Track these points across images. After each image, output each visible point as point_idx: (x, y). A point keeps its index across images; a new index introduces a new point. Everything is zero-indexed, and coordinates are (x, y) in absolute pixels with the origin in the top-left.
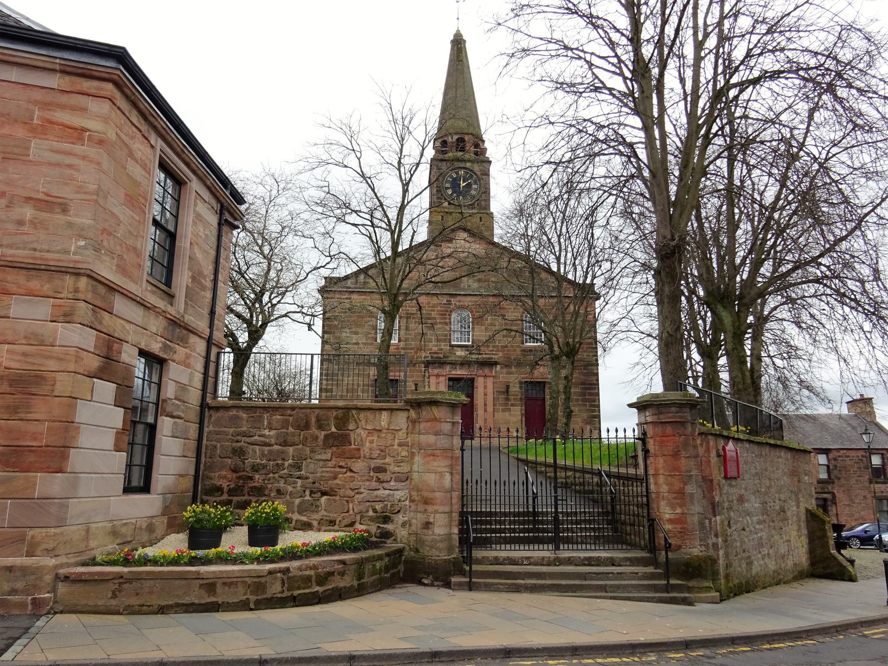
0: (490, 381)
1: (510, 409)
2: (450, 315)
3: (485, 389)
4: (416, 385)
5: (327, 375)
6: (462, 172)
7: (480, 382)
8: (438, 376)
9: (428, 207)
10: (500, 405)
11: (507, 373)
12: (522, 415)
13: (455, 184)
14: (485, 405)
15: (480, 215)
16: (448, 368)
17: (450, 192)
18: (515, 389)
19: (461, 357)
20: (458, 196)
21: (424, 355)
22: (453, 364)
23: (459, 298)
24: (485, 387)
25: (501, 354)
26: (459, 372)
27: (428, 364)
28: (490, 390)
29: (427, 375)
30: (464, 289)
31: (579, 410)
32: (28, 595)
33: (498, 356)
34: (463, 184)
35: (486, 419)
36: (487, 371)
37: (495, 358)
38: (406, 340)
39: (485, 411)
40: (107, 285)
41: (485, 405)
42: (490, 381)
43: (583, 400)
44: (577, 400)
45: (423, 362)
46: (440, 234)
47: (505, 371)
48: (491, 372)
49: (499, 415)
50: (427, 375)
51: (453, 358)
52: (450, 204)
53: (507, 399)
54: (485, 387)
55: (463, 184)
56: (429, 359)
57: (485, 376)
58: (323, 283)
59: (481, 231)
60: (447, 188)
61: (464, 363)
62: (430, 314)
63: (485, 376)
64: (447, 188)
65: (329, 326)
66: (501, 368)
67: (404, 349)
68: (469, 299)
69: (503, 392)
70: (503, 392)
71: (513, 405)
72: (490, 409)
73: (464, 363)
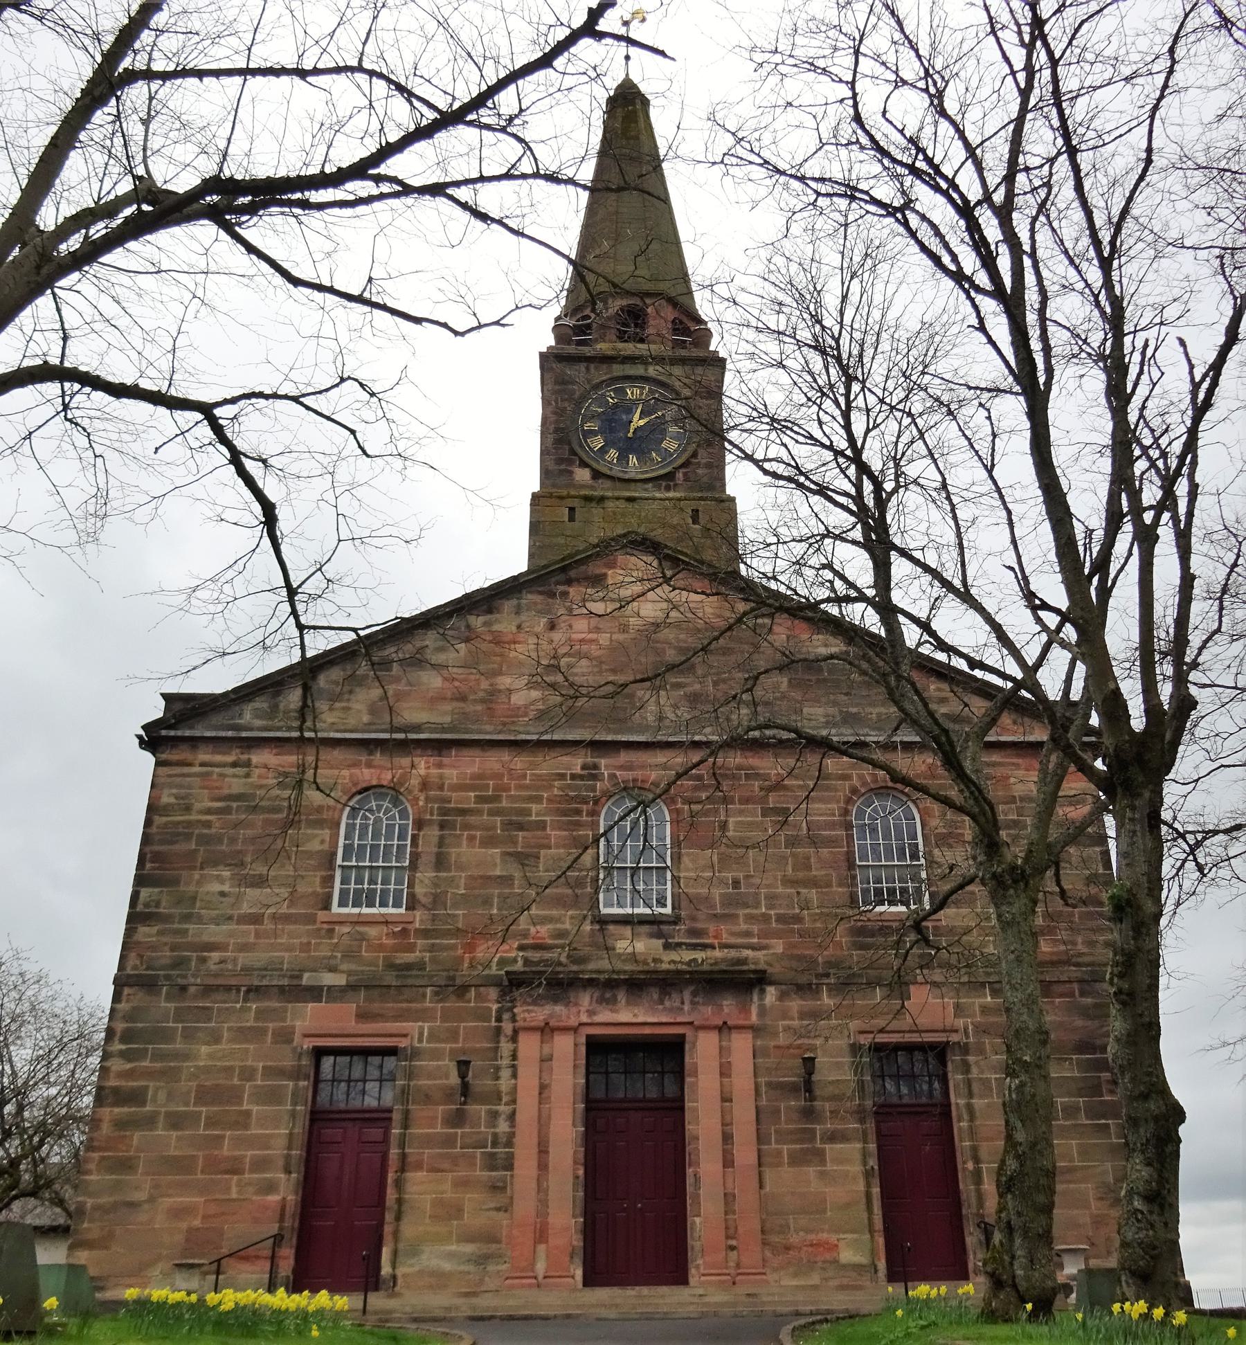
0: (741, 1045)
1: (820, 1155)
2: (594, 813)
3: (722, 1079)
4: (463, 1066)
5: (127, 1037)
6: (632, 393)
7: (703, 1052)
8: (547, 1030)
9: (664, 165)
10: (782, 1137)
11: (802, 1015)
12: (868, 1174)
13: (613, 423)
14: (727, 1138)
15: (694, 504)
16: (586, 999)
17: (598, 443)
18: (836, 1069)
19: (633, 957)
20: (623, 458)
21: (511, 954)
22: (610, 986)
23: (624, 757)
24: (725, 1071)
25: (778, 946)
26: (630, 1016)
27: (514, 984)
28: (742, 1082)
29: (508, 1027)
30: (642, 729)
31: (1084, 1152)
32: (462, 871)
33: (768, 954)
34: (638, 421)
35: (729, 1198)
36: (728, 1006)
37: (757, 958)
38: (437, 900)
39: (728, 1162)
40: (911, 1113)
41: (727, 1138)
42: (741, 1045)
43: (1092, 1113)
44: (1071, 1111)
45: (495, 982)
46: (557, 570)
47: (795, 1004)
48: (745, 1010)
49: (782, 1179)
50: (508, 1027)
51: (604, 964)
52: (597, 475)
53: (809, 1114)
54: (725, 1071)
55: (638, 421)
56: (519, 966)
57: (724, 1029)
58: (156, 710)
59: (702, 546)
60: (589, 434)
61: (639, 983)
62: (528, 812)
63: (724, 1029)
64: (589, 434)
65: (158, 857)
66: (782, 996)
67: (425, 933)
68: (660, 757)
69: (793, 1089)
70: (793, 1089)
71: (832, 1137)
72: (745, 1154)
73: (639, 983)
